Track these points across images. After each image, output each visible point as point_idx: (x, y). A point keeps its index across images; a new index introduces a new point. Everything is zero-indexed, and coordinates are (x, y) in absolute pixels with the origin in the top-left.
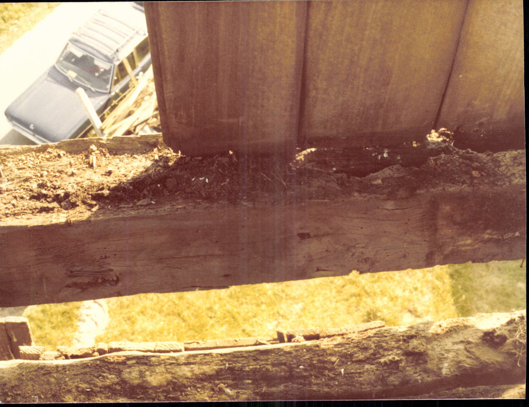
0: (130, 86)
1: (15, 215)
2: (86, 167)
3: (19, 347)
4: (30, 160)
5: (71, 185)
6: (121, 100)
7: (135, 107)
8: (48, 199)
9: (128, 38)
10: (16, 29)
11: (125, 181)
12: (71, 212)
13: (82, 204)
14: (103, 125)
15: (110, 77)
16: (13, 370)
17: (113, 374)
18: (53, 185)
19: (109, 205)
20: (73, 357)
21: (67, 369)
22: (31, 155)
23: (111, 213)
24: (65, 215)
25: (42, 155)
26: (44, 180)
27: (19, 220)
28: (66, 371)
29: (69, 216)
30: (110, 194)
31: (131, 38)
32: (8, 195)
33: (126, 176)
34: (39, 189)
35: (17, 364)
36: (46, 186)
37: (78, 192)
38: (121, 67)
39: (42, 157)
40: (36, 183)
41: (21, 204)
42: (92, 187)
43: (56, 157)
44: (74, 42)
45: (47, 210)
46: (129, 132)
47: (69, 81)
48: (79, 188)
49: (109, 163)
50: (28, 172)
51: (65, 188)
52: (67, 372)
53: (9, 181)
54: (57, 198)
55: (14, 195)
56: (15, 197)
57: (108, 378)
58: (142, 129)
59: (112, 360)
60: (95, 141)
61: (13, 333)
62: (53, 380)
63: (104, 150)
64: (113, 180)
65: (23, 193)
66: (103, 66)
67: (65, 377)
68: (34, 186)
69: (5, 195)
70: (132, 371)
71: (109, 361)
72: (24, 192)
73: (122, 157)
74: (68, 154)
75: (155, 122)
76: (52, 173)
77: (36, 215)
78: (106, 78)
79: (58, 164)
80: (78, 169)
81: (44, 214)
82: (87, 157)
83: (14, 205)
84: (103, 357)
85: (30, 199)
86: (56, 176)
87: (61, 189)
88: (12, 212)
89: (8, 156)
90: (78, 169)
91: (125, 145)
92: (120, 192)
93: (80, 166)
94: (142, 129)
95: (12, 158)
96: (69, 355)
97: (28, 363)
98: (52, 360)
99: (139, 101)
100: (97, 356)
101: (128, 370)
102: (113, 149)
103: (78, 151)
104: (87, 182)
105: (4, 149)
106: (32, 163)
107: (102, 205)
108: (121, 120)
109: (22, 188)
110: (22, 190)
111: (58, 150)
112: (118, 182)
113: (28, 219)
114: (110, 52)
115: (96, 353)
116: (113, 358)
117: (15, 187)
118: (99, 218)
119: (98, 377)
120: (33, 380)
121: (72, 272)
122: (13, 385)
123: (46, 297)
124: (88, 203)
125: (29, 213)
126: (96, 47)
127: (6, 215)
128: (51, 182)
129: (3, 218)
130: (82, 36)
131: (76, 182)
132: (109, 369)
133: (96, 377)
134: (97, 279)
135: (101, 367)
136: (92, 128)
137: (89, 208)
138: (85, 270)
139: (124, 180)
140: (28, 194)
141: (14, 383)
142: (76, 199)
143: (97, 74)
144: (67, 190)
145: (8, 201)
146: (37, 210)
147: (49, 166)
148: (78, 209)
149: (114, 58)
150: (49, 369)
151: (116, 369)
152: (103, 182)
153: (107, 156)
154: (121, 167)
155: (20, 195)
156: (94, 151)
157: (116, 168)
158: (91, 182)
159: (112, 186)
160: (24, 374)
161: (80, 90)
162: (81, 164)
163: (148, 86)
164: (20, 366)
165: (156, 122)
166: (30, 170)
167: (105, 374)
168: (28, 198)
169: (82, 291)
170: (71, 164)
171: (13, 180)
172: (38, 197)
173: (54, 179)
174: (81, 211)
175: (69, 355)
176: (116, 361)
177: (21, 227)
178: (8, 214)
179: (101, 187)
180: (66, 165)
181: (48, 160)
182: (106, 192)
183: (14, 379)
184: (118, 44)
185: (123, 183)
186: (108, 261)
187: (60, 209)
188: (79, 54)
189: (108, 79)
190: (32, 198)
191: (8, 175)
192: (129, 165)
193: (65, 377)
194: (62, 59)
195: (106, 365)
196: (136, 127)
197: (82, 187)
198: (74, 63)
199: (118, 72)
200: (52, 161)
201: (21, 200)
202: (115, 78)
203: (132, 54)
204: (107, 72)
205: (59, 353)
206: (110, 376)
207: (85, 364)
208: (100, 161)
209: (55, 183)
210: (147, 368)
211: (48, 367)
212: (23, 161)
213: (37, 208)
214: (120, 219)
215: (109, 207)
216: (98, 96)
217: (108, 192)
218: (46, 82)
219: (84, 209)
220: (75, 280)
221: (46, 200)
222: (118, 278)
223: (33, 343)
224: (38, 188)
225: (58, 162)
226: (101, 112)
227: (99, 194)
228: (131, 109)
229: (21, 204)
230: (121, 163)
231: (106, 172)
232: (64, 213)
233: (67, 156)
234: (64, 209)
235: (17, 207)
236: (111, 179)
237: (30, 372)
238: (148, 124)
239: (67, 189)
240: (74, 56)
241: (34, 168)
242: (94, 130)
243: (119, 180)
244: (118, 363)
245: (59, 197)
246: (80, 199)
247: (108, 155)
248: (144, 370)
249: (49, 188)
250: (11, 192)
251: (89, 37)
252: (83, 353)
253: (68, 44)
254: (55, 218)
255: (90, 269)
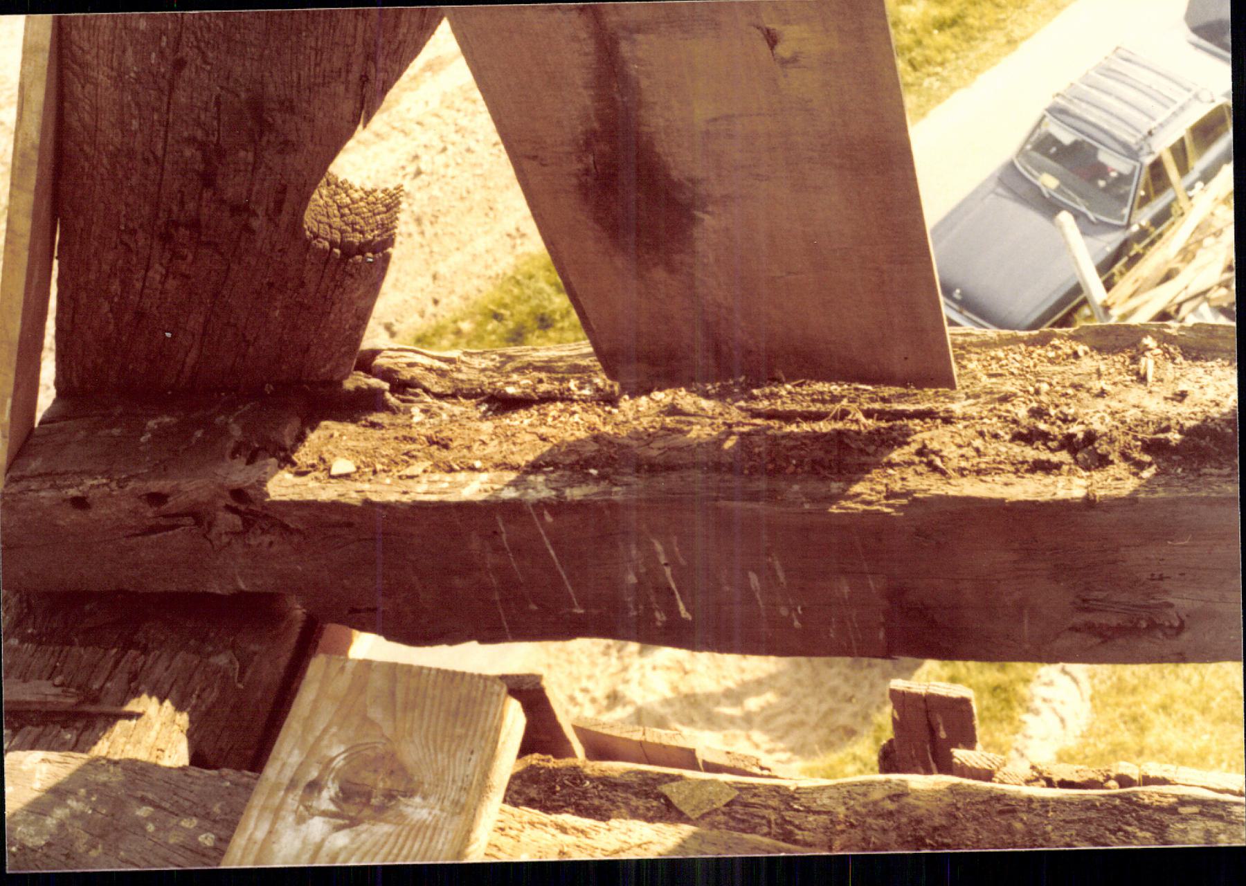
0: (1173, 211)
1: (979, 472)
2: (1132, 381)
3: (952, 750)
4: (1014, 359)
5: (1098, 415)
6: (1152, 243)
7: (1182, 261)
8: (1050, 444)
9: (1174, 108)
10: (937, 84)
11: (1217, 416)
12: (1097, 475)
13: (1121, 459)
14: (1109, 298)
15: (1129, 191)
16: (939, 796)
17: (1148, 830)
18: (1061, 412)
19: (1179, 466)
20: (1064, 784)
21: (1050, 808)
22: (1017, 350)
23: (1182, 486)
24: (1084, 482)
25: (1039, 351)
26: (1040, 402)
27: (989, 485)
28: (1047, 812)
29: (1092, 485)
30: (1183, 441)
31: (1182, 108)
32: (965, 427)
33: (1217, 405)
34: (1032, 420)
35: (946, 785)
36: (1048, 414)
37: (1115, 433)
38: (1157, 168)
39: (1040, 355)
40: (1024, 406)
41: (992, 448)
42: (1143, 423)
43: (1068, 356)
44: (1059, 116)
45: (1046, 467)
46: (1164, 316)
47: (1044, 197)
48: (1116, 423)
49: (1182, 375)
50: (1009, 383)
51: (1086, 422)
52: (1051, 814)
53: (968, 397)
54: (1069, 443)
55: (978, 428)
56: (981, 434)
57: (1135, 837)
58: (1194, 310)
59: (1147, 801)
60: (1155, 329)
61: (939, 719)
62: (1018, 826)
63: (1171, 349)
64: (1189, 411)
65: (994, 424)
66: (1116, 164)
67: (1046, 822)
68: (1022, 412)
69: (960, 426)
70: (1189, 828)
71: (1141, 801)
72: (999, 425)
73: (1209, 364)
74: (1094, 353)
75: (1226, 296)
76: (1059, 388)
77: (1023, 477)
78: (1122, 191)
79: (1072, 371)
80: (1115, 384)
81: (1039, 475)
82: (1135, 360)
83: (977, 450)
84: (1129, 793)
85: (1012, 440)
86: (1067, 394)
87: (1079, 423)
88: (973, 466)
89: (969, 348)
90: (1115, 384)
91: (1218, 340)
92: (1204, 439)
93: (1118, 378)
94: (1194, 310)
95: (977, 353)
96: (1056, 779)
97: (969, 786)
98: (1020, 785)
99: (1191, 248)
100: (1114, 788)
101: (1181, 826)
102: (1193, 349)
103: (1116, 347)
104: (1133, 411)
105: (962, 335)
106: (1018, 365)
107: (1165, 464)
108: (1151, 288)
109: (996, 415)
110: (995, 419)
111: (1073, 344)
112: (1200, 416)
113: (1006, 484)
114: (1134, 136)
115: (1112, 783)
116: (1150, 796)
117: (981, 412)
118: (1156, 496)
119: (1114, 832)
120: (977, 820)
121: (1084, 601)
122: (937, 824)
123: (1027, 646)
124: (1134, 459)
125: (1009, 472)
126: (1106, 126)
127: (961, 472)
128: (1057, 406)
129: (954, 478)
130: (1076, 101)
131: (1109, 410)
132: (1139, 819)
133: (1110, 830)
134: (1139, 619)
135: (1121, 812)
136: (1085, 302)
137: (1135, 470)
138: (1115, 599)
139: (1214, 412)
140: (1007, 430)
141: (938, 821)
142: (1109, 448)
143: (1102, 183)
144: (1091, 427)
145: (966, 440)
146: (1026, 466)
147: (1054, 374)
148: (1111, 470)
149: (1141, 148)
150: (1013, 803)
151: (1155, 820)
152: (1169, 415)
153: (1177, 361)
154: (1208, 385)
155: (991, 430)
156: (1150, 350)
157: (1197, 386)
158: (1142, 412)
159: (1189, 424)
160: (959, 805)
161: (1065, 218)
162: (1120, 374)
163: (1212, 214)
164: (953, 789)
165: (1228, 296)
166: (1014, 380)
167: (1129, 829)
168: (1008, 437)
169: (1103, 642)
170: (1099, 374)
171: (977, 396)
172: (1029, 437)
173: (1063, 400)
174: (1118, 476)
175: (1056, 779)
176: (1156, 804)
177: (991, 500)
178: (964, 469)
179: (1164, 424)
180: (1089, 374)
181: (1051, 361)
182: (1174, 437)
183: (940, 815)
184: (1153, 119)
185: (1213, 420)
186: (1165, 585)
187: (1073, 467)
188: (1067, 138)
189: (1127, 194)
190: (1017, 437)
191: (968, 386)
192: (1223, 383)
193: (1046, 822)
194: (1029, 147)
195: (1134, 810)
196: (1180, 305)
197: (1123, 422)
198: (1054, 157)
199: (1150, 182)
200: (1059, 364)
201: (994, 440)
202: (1142, 193)
203: (1182, 140)
204: (1123, 179)
205: (1035, 774)
206: (1140, 834)
207: (1088, 801)
208: (1161, 371)
209: (1065, 409)
210: (1222, 828)
211: (1011, 799)
212: (999, 360)
213: (1027, 462)
214: (1202, 501)
215: (1179, 470)
216: (1104, 232)
217: (1178, 436)
218: (992, 196)
219: (1124, 472)
220: (1089, 617)
221: (1045, 444)
222: (1182, 622)
223: (979, 746)
224: (1030, 417)
225: (1073, 367)
226: (1107, 269)
227: (1160, 440)
228: (1173, 265)
229: (993, 449)
230: (1208, 377)
231: (1175, 394)
232: (1082, 477)
233: (1092, 357)
234: (1083, 469)
235: (985, 455)
236: (1184, 409)
237: (973, 804)
238: (1208, 300)
239: (1091, 424)
240: (1056, 142)
241: (1023, 373)
242: (1089, 306)
243: (1203, 412)
244: (1160, 809)
245: (1074, 440)
246: (1116, 448)
247: (1180, 359)
248: (1215, 830)
249: (1053, 420)
250: (972, 421)
251: (1088, 103)
252: (1085, 779)
253: (1044, 117)
254: (1063, 487)
255: (1124, 597)
